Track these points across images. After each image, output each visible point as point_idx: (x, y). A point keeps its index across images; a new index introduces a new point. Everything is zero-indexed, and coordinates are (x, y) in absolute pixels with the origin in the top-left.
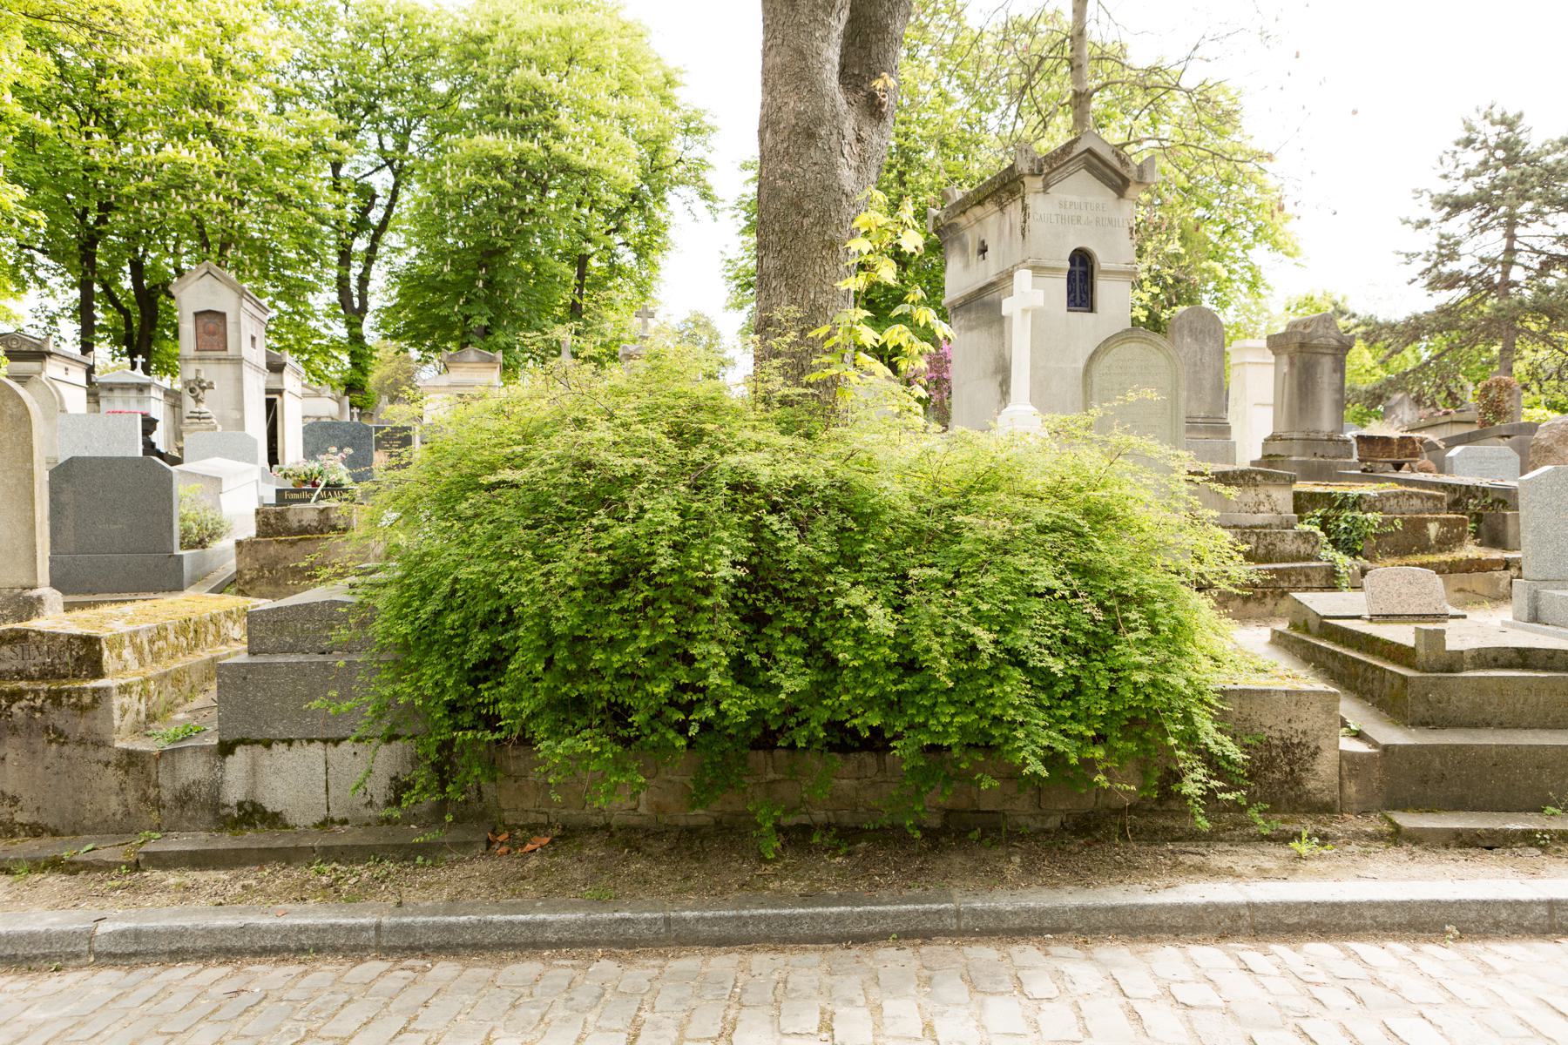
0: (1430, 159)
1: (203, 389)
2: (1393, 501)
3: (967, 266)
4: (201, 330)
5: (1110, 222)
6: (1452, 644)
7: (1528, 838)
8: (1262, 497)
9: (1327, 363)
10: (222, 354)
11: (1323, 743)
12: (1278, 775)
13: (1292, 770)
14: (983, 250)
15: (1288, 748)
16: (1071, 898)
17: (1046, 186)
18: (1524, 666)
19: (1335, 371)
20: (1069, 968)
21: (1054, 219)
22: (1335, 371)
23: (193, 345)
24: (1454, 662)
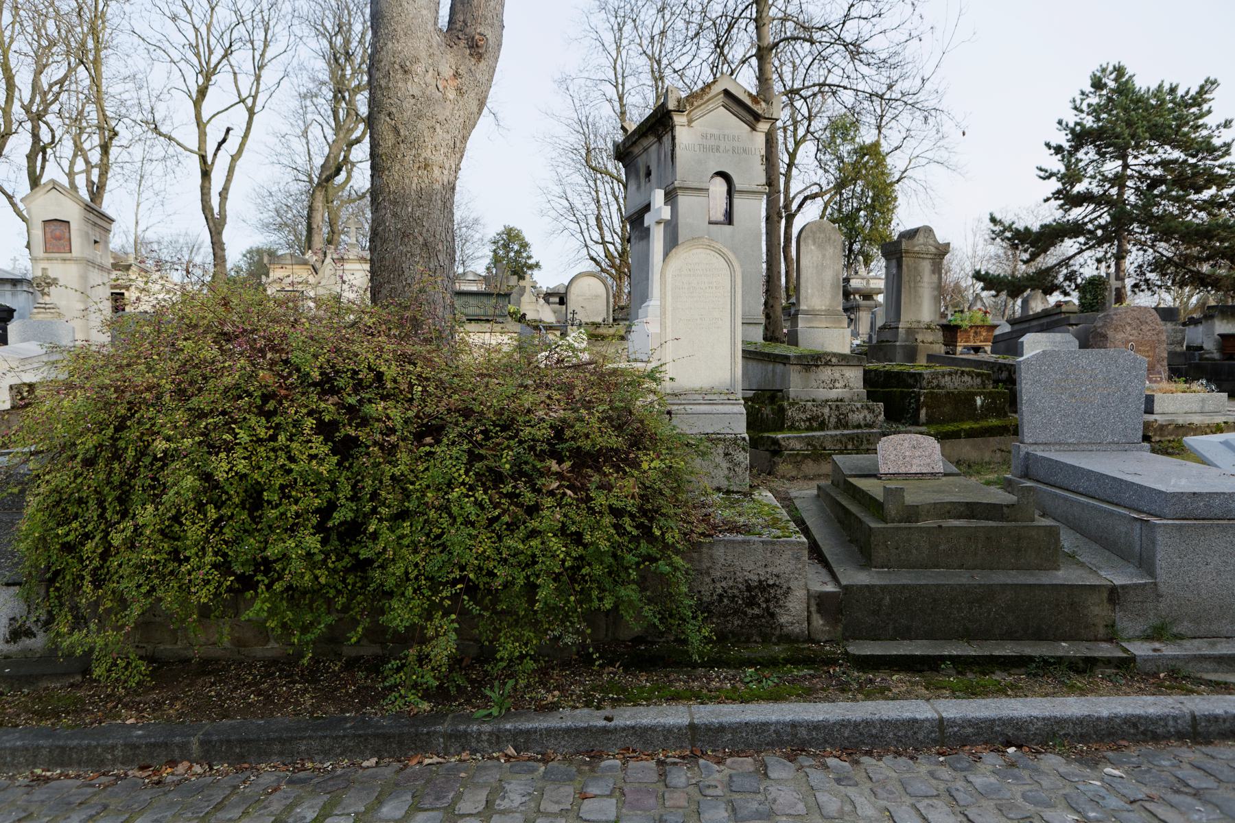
0: (1055, 100)
1: (49, 285)
2: (947, 378)
3: (639, 187)
4: (49, 235)
5: (744, 151)
6: (909, 499)
7: (1008, 663)
8: (837, 375)
9: (926, 266)
10: (68, 255)
11: (793, 584)
12: (756, 611)
13: (768, 607)
14: (648, 174)
15: (763, 587)
16: (675, 716)
17: (690, 122)
18: (971, 516)
19: (933, 272)
20: (1178, 751)
21: (697, 148)
22: (933, 272)
23: (42, 248)
24: (912, 513)
